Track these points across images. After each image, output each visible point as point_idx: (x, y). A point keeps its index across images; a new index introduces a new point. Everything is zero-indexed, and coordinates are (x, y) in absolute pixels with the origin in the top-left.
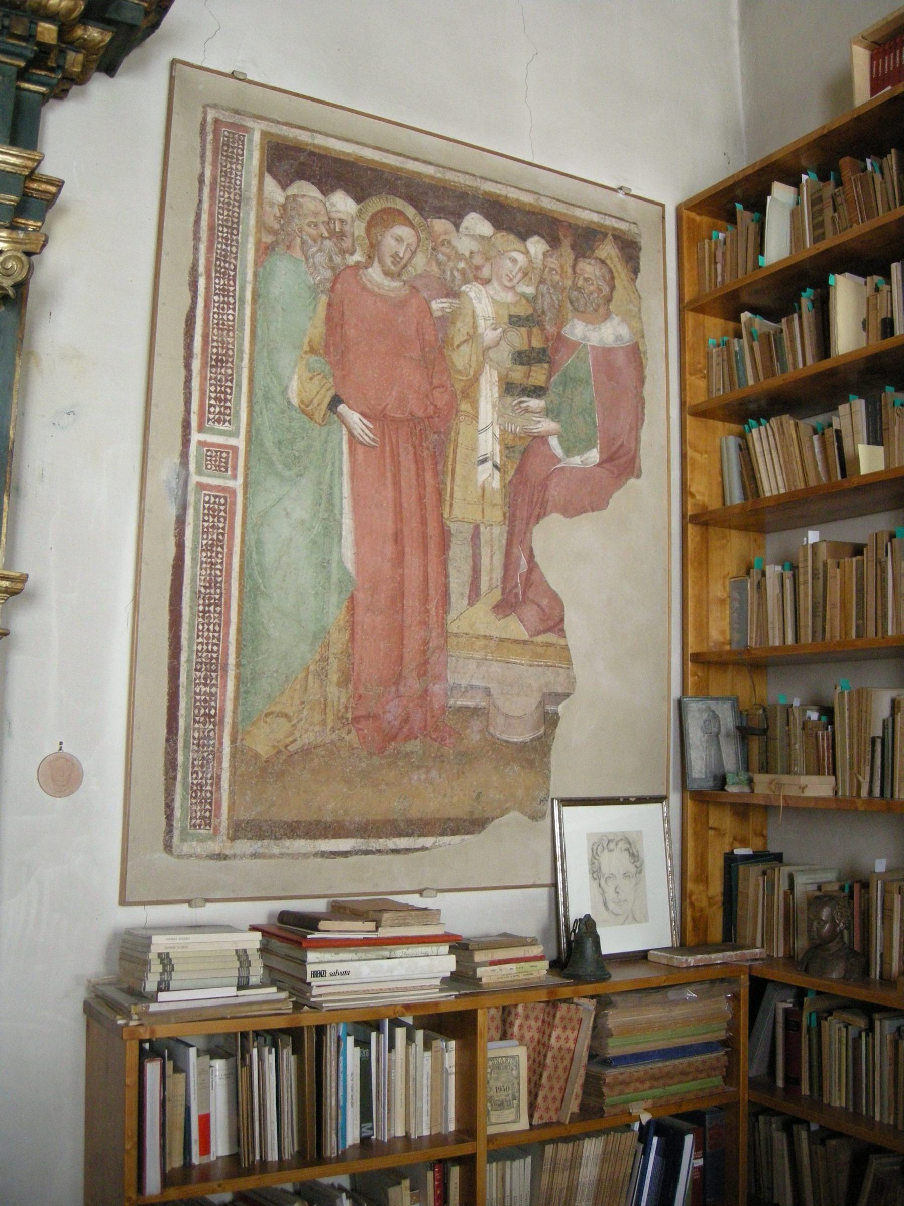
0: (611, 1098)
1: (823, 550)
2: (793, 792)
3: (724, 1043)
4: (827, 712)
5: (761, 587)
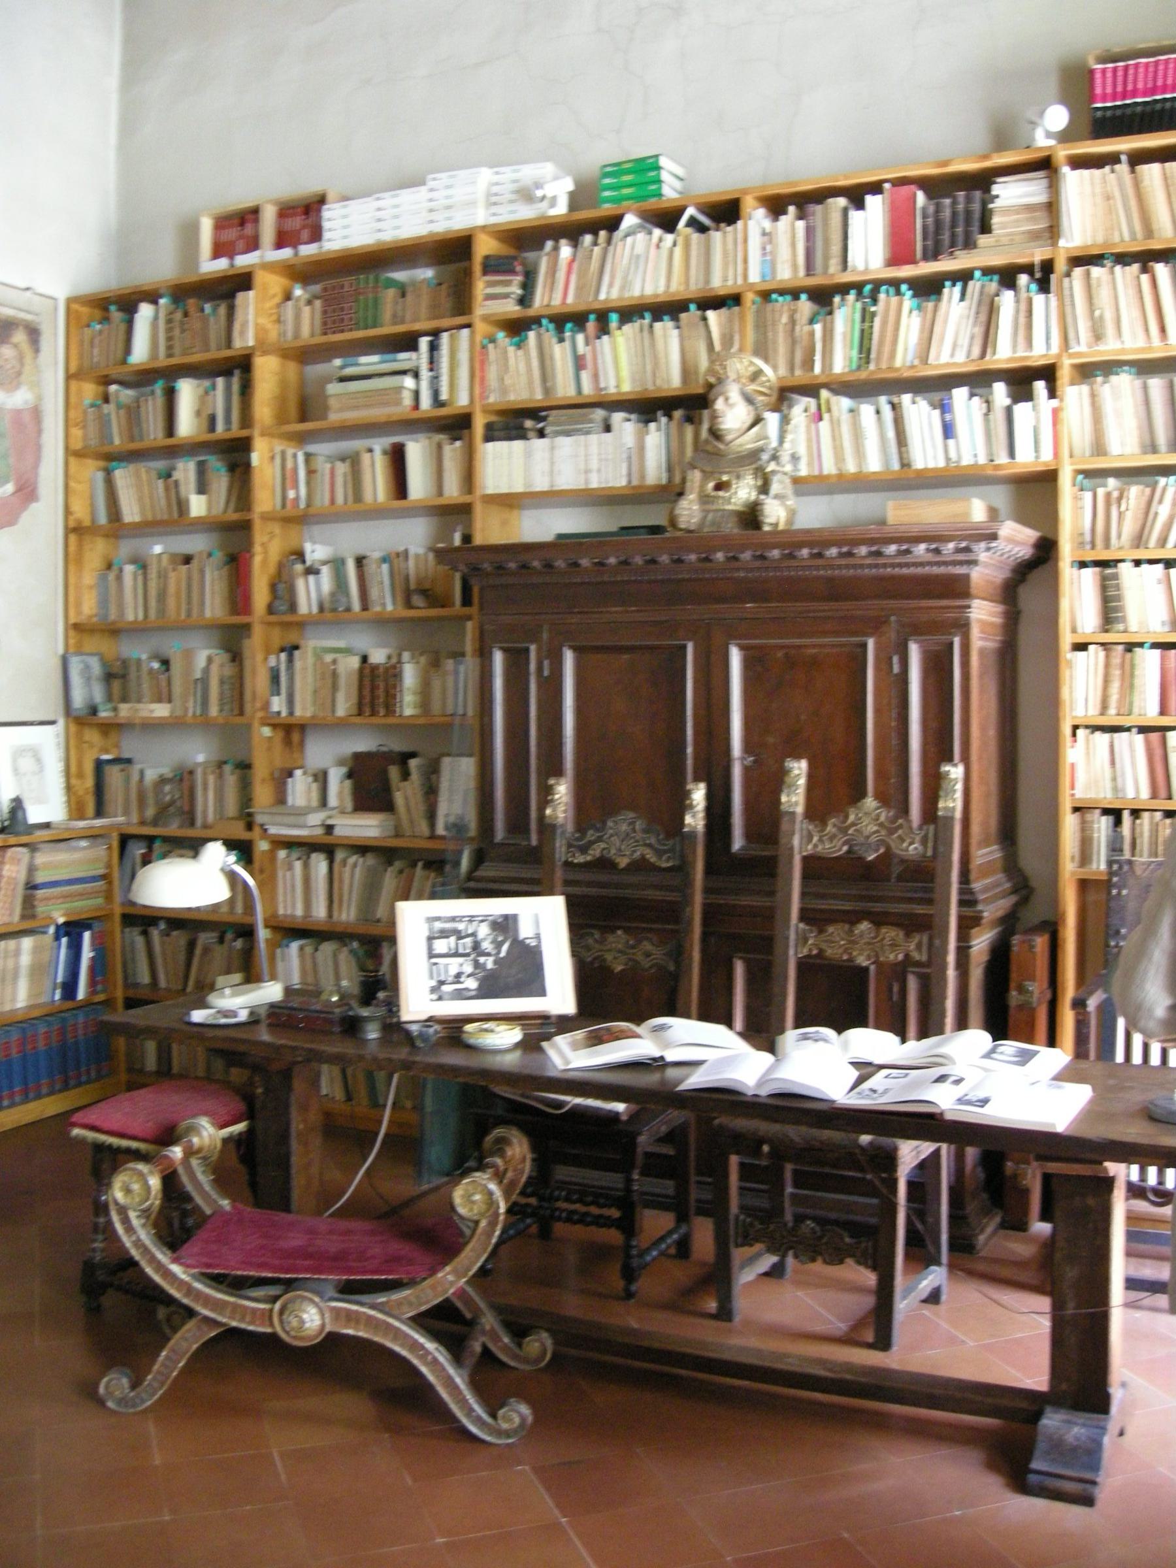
0: (41, 909)
1: (165, 558)
2: (145, 714)
3: (103, 877)
4: (166, 663)
5: (119, 578)
